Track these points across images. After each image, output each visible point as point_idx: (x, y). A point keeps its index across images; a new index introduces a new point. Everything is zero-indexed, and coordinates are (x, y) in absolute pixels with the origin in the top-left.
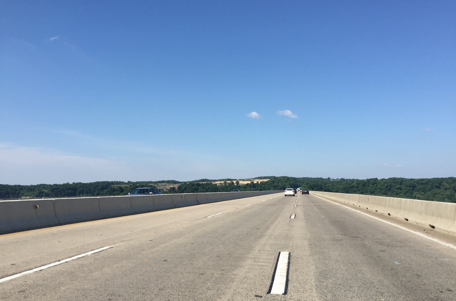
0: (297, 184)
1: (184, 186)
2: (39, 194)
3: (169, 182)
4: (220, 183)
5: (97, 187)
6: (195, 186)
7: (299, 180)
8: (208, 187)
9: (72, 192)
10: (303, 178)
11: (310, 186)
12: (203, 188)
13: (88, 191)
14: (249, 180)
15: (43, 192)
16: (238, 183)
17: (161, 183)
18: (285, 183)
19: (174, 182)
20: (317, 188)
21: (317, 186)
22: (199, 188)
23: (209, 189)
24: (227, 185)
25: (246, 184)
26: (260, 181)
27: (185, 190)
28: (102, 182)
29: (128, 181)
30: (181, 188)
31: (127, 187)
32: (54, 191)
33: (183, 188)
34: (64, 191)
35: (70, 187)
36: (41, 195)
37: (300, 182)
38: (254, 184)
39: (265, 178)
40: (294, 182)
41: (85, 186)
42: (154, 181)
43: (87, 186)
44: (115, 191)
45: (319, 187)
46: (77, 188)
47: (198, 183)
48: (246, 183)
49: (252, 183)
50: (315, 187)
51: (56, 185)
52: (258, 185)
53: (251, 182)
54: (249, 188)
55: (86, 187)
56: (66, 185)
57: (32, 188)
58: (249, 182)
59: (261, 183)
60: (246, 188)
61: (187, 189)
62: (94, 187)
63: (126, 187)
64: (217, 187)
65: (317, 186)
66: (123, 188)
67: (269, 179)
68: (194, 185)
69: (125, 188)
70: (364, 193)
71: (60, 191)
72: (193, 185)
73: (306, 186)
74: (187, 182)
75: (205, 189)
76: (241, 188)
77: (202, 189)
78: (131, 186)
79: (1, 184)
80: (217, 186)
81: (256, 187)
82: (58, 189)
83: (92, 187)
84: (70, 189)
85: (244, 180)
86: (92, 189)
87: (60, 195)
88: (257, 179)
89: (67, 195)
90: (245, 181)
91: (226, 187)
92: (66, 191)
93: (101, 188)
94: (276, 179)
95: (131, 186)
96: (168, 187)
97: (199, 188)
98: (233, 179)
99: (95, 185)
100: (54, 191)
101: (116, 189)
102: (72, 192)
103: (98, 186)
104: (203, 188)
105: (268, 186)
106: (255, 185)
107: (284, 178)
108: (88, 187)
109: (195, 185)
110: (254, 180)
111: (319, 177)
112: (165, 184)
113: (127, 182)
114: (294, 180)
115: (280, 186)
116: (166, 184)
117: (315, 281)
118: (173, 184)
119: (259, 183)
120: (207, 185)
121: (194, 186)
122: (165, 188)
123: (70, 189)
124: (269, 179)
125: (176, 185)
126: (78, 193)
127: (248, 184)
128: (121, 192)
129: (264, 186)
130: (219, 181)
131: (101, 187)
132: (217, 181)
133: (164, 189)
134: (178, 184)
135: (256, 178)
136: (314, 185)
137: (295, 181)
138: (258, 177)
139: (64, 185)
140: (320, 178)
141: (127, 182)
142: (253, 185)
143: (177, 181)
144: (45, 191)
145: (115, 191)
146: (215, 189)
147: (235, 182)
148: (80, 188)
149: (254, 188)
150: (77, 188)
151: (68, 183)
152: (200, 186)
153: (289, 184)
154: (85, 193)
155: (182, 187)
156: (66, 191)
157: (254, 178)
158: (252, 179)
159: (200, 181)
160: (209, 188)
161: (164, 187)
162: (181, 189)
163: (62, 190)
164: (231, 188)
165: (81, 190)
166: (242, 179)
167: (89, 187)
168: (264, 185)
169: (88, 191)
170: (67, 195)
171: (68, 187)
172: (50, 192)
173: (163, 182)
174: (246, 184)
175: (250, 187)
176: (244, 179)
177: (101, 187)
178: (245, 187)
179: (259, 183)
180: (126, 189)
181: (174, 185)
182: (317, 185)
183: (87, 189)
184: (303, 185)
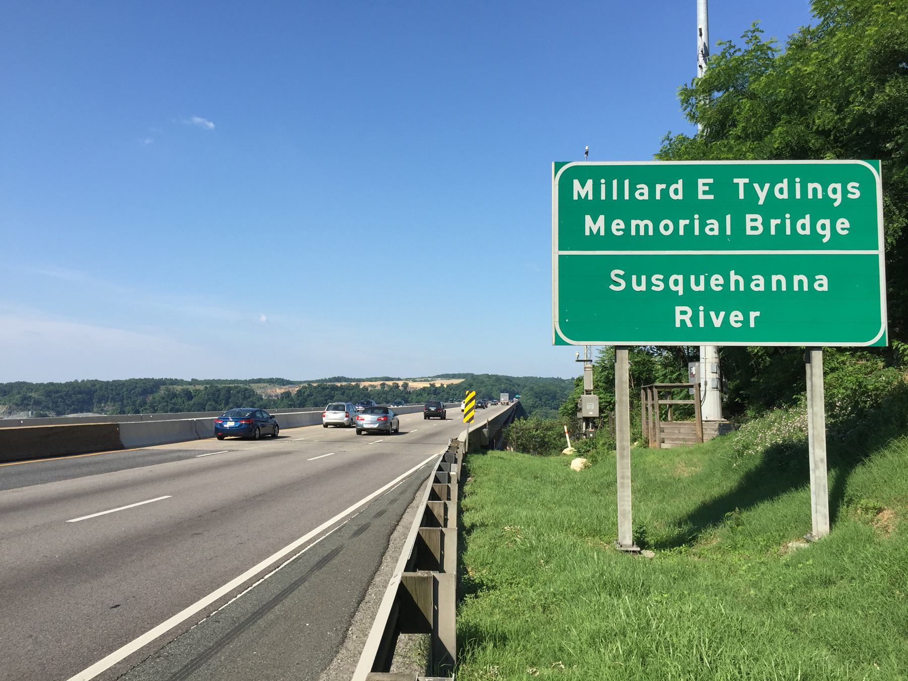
0: (514, 390)
1: (308, 390)
2: (23, 401)
3: (272, 382)
4: (371, 385)
5: (134, 389)
6: (328, 390)
7: (517, 382)
8: (352, 392)
9: (86, 398)
10: (525, 378)
11: (536, 393)
12: (343, 395)
13: (115, 397)
14: (425, 381)
15: (30, 397)
16: (406, 386)
17: (257, 383)
18: (491, 387)
19: (282, 382)
20: (547, 397)
21: (546, 394)
22: (336, 393)
23: (354, 397)
24: (386, 389)
25: (422, 387)
26: (446, 383)
27: (310, 397)
28: (141, 380)
29: (192, 379)
30: (302, 393)
31: (199, 391)
32: (50, 396)
33: (305, 394)
34: (70, 397)
35: (82, 388)
36: (25, 402)
37: (519, 385)
38: (437, 388)
39: (454, 376)
40: (507, 386)
41: (109, 388)
42: (243, 379)
43: (114, 388)
44: (177, 397)
45: (551, 396)
46: (95, 391)
47: (334, 385)
48: (420, 385)
49: (433, 385)
50: (544, 395)
51: (52, 384)
52: (444, 391)
53: (430, 384)
54: (426, 395)
55: (112, 390)
56: (74, 385)
57: (5, 389)
58: (427, 385)
59: (448, 386)
60: (422, 395)
61: (313, 395)
62: (127, 389)
63: (197, 390)
64: (368, 393)
65: (546, 394)
66: (192, 392)
67: (463, 380)
68: (327, 388)
69: (196, 393)
70: (287, 395)
71: (62, 395)
72: (324, 388)
73: (529, 394)
74: (313, 382)
75: (347, 396)
76: (413, 395)
77: (342, 396)
78: (207, 388)
79: (5, 380)
80: (367, 390)
81: (439, 393)
82: (58, 392)
83: (125, 389)
84: (80, 393)
85: (414, 380)
86: (125, 393)
87: (62, 403)
88: (439, 379)
89: (76, 403)
90: (416, 383)
91: (384, 393)
92: (73, 396)
93: (141, 391)
94: (475, 380)
95: (206, 388)
96: (269, 391)
97: (336, 393)
98: (395, 378)
99: (130, 385)
100: (50, 396)
101: (179, 394)
102: (86, 398)
103: (136, 387)
104: (343, 394)
105: (462, 392)
106: (438, 390)
107: (489, 378)
108: (116, 388)
109: (328, 388)
110: (433, 379)
111: (554, 377)
112: (265, 385)
113: (190, 381)
114: (508, 382)
115: (483, 392)
116: (267, 384)
117: (4, 535)
118: (281, 385)
119: (445, 386)
120: (349, 390)
121: (327, 391)
122: (264, 393)
123: (80, 393)
124: (463, 380)
125: (285, 387)
126: (97, 400)
127: (424, 389)
128: (188, 401)
129: (454, 392)
130: (367, 381)
131: (141, 389)
132: (364, 380)
133: (263, 394)
134: (290, 385)
135: (438, 377)
136: (543, 391)
137: (510, 385)
138: (442, 375)
139: (68, 385)
140: (556, 377)
141: (190, 381)
142: (434, 390)
143: (286, 380)
144: (33, 394)
145: (177, 397)
146: (365, 396)
147: (400, 383)
148: (101, 390)
149: (435, 396)
150: (95, 391)
151: (76, 381)
152: (337, 390)
153: (499, 390)
154: (109, 400)
155: (304, 393)
156: (73, 396)
157: (434, 377)
158: (429, 377)
159: (330, 380)
160: (353, 394)
161: (263, 390)
162: (301, 395)
163: (66, 395)
164: (394, 396)
165: (102, 394)
166: (411, 379)
167: (118, 389)
168: (454, 390)
169: (115, 397)
170: (76, 403)
171: (77, 389)
172: (43, 398)
173: (259, 381)
174: (421, 389)
175: (428, 395)
176: (415, 378)
177: (141, 389)
178: (419, 394)
179: (445, 386)
180: (198, 395)
181: (283, 387)
182: (548, 392)
183: (114, 392)
184: (522, 392)
